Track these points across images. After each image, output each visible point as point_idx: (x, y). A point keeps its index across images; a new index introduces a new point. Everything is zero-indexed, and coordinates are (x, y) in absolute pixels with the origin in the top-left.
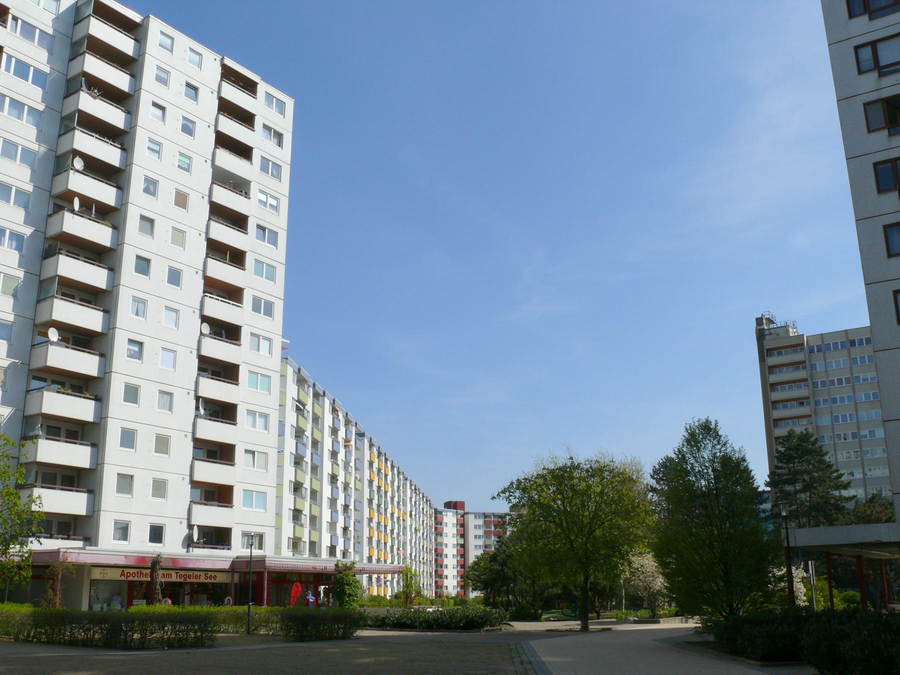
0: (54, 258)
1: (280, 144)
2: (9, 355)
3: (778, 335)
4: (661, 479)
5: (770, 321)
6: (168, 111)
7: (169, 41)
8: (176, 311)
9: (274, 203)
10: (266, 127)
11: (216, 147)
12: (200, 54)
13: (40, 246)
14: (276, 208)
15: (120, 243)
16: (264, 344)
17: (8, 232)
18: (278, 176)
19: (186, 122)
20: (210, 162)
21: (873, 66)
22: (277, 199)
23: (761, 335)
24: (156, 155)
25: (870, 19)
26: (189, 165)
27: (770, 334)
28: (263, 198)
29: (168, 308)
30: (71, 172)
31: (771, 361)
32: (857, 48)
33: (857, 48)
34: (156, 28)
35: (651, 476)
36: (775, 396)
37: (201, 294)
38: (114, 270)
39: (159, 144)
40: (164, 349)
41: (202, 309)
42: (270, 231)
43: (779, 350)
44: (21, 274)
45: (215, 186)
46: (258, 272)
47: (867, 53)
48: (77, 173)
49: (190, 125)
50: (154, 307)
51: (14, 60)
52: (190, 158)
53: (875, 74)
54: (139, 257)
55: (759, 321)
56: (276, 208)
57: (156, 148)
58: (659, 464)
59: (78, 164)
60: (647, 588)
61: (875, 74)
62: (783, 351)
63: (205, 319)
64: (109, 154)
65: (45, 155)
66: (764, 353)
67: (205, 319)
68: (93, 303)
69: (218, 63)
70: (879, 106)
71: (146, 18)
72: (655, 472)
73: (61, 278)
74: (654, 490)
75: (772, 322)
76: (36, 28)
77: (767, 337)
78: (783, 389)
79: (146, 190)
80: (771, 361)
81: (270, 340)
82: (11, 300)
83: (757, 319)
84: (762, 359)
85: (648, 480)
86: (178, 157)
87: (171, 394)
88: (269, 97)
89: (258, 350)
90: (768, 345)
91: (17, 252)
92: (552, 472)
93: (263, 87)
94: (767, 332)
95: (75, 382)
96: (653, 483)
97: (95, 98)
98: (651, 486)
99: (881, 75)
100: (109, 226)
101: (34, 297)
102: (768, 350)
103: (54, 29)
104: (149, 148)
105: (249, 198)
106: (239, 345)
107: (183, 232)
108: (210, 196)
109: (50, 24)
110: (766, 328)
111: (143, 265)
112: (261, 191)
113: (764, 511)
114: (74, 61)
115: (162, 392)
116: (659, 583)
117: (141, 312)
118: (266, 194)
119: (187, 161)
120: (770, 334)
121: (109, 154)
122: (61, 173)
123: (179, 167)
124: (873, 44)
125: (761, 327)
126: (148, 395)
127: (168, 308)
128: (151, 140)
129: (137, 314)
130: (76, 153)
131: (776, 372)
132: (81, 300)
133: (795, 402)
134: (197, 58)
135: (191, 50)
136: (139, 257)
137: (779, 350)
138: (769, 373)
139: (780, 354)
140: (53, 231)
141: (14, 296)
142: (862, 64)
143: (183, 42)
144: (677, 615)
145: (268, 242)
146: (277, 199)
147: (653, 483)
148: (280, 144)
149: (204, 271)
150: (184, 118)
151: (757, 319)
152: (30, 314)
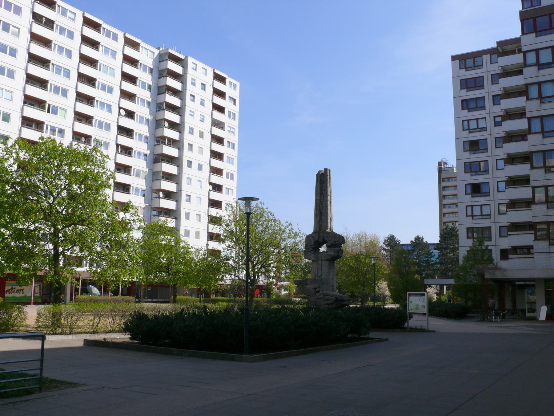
0: (159, 164)
1: (234, 104)
2: (145, 203)
3: (448, 171)
4: (388, 245)
5: (445, 163)
6: (196, 97)
7: (195, 66)
8: (201, 181)
9: (232, 130)
10: (230, 97)
11: (212, 110)
12: (206, 69)
13: (152, 158)
14: (233, 133)
15: (181, 155)
16: (230, 191)
17: (142, 153)
18: (234, 119)
19: (202, 101)
20: (210, 117)
21: (467, 129)
22: (234, 129)
23: (440, 171)
24: (192, 117)
25: (468, 111)
26: (203, 119)
27: (445, 170)
28: (229, 129)
29: (198, 181)
30: (164, 128)
31: (444, 184)
32: (463, 121)
33: (463, 121)
34: (191, 61)
35: (383, 243)
36: (445, 202)
37: (209, 173)
38: (179, 166)
39: (193, 112)
40: (197, 197)
41: (209, 180)
42: (232, 143)
43: (448, 179)
44: (147, 170)
45: (125, 46)
46: (228, 162)
47: (466, 123)
48: (166, 129)
49: (203, 101)
50: (194, 180)
51: (141, 82)
52: (203, 116)
53: (468, 131)
54: (188, 161)
55: (440, 164)
56: (233, 133)
57: (192, 114)
58: (387, 238)
59: (166, 124)
60: (382, 294)
61: (468, 131)
62: (450, 179)
63: (211, 184)
64: (175, 118)
65: (153, 120)
66: (441, 180)
67: (211, 184)
68: (170, 179)
69: (212, 72)
70: (468, 143)
71: (187, 57)
72: (386, 241)
73: (162, 171)
74: (384, 249)
75: (446, 164)
76: (147, 66)
77: (443, 172)
78: (449, 199)
79: (190, 133)
80: (444, 184)
81: (232, 190)
82: (144, 181)
83: (439, 163)
84: (440, 183)
85: (381, 244)
86: (200, 116)
87: (200, 215)
88: (231, 83)
89: (228, 194)
90: (443, 176)
91: (145, 161)
92: (354, 256)
93: (228, 80)
94: (443, 169)
95: (165, 211)
96: (384, 246)
97: (170, 95)
98: (383, 248)
99: (469, 132)
100: (176, 148)
101: (151, 179)
102: (443, 179)
103: (153, 66)
104: (190, 114)
105: (224, 130)
106: (222, 193)
107: (202, 148)
108: (211, 131)
109: (152, 63)
110: (443, 167)
111: (190, 164)
112: (229, 126)
113: (432, 261)
114: (161, 79)
115: (197, 214)
116: (387, 293)
117: (189, 183)
118: (230, 127)
119: (202, 117)
120: (445, 170)
121: (175, 118)
122: (159, 128)
123: (200, 121)
124: (468, 121)
125: (440, 167)
126: (193, 216)
127: (198, 181)
128: (191, 111)
129: (188, 184)
130: (165, 120)
131: (446, 190)
132: (30, 104)
133: (454, 205)
134: (204, 71)
135: (203, 68)
136: (188, 161)
137: (448, 179)
138: (443, 190)
139: (449, 181)
140: (158, 152)
141: (145, 179)
142: (464, 127)
143: (200, 65)
144: (392, 303)
145: (231, 148)
146: (234, 129)
147: (384, 246)
148: (234, 104)
149: (210, 164)
150: (201, 99)
151: (439, 163)
152: (150, 186)
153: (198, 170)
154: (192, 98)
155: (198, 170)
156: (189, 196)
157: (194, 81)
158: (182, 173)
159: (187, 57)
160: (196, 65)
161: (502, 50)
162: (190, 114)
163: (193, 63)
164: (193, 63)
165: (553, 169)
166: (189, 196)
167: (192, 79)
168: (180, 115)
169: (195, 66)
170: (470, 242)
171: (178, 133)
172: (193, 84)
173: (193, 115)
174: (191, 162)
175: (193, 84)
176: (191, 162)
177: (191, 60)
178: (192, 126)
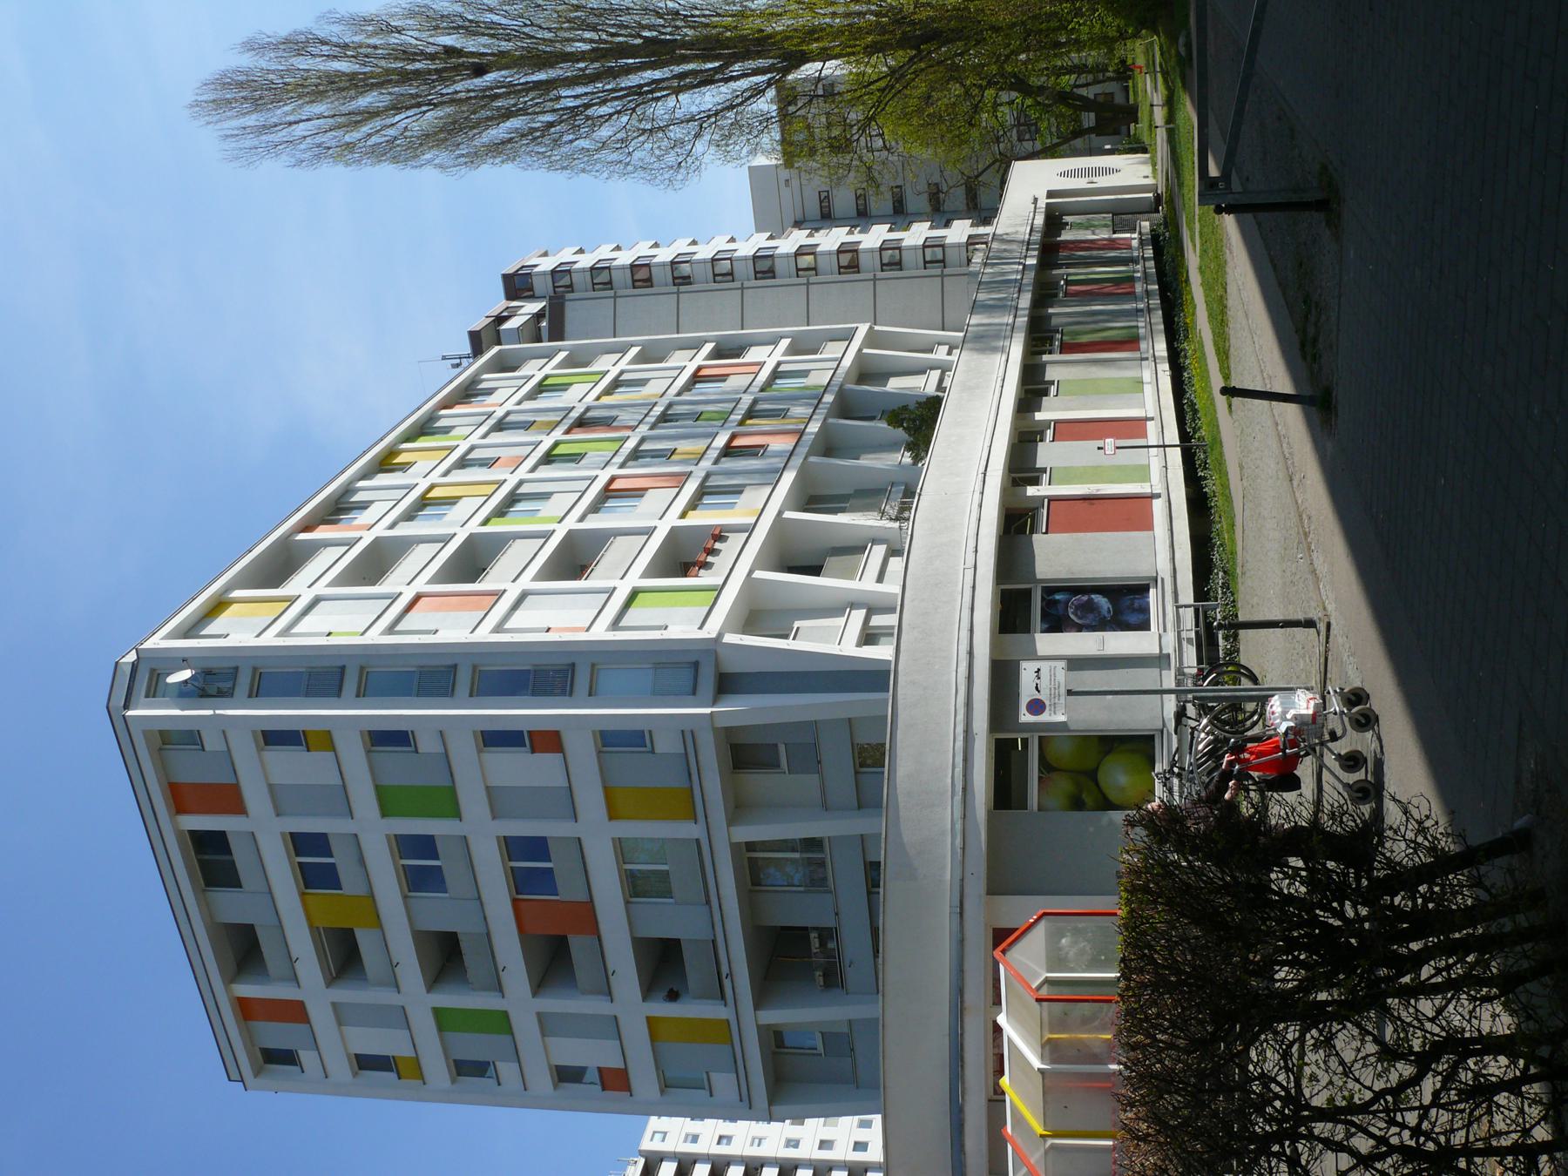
57: (757, 1141)
104: (759, 1145)
142: (1251, 632)
153: (870, 1127)
154: (725, 1141)
155: (870, 1127)
156: (721, 1138)
157: (690, 1138)
158: (810, 1160)
159: (640, 1151)
160: (654, 1132)
161: (1067, 224)
162: (759, 1145)
163: (652, 1140)
164: (652, 1140)
165: (1567, 1097)
166: (721, 1138)
167: (685, 1141)
168: (762, 1166)
169: (656, 1135)
170: (1091, 96)
171: (697, 1165)
172: (695, 1138)
173: (760, 1140)
174: (856, 1143)
175: (695, 1138)
176: (856, 1143)
177: (647, 1145)
178: (783, 1142)
